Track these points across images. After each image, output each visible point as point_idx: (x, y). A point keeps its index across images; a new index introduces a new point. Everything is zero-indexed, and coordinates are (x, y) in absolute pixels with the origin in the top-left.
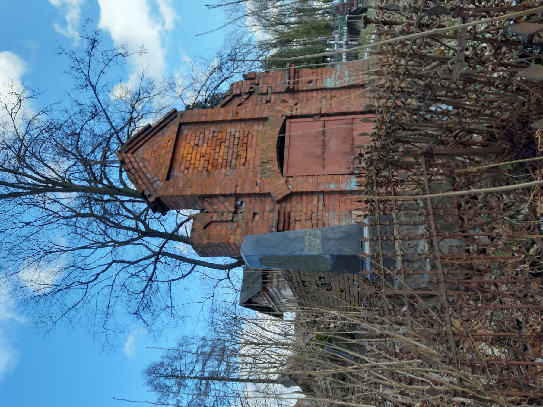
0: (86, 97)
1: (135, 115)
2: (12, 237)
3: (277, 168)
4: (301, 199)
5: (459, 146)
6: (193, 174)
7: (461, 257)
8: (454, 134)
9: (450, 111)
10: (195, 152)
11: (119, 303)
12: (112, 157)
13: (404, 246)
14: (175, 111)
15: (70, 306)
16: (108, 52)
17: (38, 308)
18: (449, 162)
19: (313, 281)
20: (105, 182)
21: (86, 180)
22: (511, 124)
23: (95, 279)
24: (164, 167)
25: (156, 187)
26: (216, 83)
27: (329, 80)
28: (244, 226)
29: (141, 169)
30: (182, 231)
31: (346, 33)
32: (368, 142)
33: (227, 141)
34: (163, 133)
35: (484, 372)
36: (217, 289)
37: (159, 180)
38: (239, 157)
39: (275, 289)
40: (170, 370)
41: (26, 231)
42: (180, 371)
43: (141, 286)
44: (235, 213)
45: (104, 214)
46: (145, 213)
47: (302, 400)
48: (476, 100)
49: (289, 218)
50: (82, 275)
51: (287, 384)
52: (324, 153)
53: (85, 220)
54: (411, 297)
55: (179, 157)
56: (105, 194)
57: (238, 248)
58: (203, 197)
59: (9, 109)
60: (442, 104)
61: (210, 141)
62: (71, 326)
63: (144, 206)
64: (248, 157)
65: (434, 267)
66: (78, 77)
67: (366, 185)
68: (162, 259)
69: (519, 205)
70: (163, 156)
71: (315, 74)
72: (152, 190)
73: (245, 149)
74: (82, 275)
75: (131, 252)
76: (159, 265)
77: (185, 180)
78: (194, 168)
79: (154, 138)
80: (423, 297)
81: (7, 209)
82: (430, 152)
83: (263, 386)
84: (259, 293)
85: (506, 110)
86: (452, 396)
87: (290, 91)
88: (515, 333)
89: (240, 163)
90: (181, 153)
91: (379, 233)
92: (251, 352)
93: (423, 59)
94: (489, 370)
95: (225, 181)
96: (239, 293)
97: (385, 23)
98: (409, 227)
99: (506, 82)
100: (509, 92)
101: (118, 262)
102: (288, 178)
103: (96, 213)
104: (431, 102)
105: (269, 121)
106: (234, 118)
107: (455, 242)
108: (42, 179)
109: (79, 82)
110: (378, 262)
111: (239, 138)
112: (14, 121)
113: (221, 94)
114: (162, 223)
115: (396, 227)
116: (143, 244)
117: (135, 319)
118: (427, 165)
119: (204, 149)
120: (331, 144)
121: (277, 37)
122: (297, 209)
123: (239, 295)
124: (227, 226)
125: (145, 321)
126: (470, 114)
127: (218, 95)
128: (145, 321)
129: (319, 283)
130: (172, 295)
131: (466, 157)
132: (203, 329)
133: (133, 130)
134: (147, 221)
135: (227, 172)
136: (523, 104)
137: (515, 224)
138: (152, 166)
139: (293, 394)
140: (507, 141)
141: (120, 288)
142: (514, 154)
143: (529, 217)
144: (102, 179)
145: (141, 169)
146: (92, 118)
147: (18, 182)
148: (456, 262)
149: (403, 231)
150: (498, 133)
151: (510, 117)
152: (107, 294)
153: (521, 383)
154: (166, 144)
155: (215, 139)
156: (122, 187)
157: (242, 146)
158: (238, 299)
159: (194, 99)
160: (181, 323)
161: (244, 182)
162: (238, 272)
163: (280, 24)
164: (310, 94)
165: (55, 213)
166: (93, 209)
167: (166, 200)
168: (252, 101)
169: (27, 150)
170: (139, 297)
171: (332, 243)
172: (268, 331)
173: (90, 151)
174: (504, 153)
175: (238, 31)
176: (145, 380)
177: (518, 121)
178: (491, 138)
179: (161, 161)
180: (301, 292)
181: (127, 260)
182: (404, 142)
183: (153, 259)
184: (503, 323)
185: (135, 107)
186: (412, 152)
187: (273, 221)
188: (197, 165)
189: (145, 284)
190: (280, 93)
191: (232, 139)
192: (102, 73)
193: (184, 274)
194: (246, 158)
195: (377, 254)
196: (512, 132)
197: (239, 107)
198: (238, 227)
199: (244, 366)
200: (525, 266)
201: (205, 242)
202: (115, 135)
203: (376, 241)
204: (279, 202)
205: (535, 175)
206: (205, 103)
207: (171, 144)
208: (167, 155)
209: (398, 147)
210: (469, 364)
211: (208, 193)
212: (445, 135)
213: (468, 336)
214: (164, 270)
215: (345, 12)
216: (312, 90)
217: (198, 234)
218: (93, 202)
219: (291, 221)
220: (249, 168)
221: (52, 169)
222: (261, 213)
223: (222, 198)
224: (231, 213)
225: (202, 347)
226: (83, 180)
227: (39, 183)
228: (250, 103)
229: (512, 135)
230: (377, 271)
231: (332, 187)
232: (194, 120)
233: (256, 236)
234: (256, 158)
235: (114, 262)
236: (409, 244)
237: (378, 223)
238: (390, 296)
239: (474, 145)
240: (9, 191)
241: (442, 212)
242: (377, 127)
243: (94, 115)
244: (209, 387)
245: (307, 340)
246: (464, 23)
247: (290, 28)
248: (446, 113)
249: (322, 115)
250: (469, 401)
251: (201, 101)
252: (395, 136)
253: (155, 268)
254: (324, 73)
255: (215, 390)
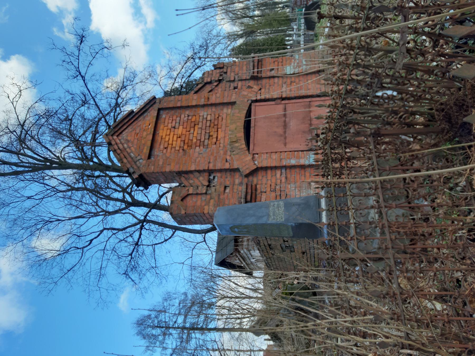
0: (77, 87)
1: (120, 100)
2: (16, 209)
3: (244, 146)
4: (266, 173)
5: (403, 126)
6: (171, 153)
7: (406, 225)
8: (399, 116)
9: (395, 96)
10: (172, 133)
11: (110, 264)
12: (100, 139)
13: (356, 214)
14: (154, 98)
15: (69, 268)
16: (95, 46)
17: (41, 270)
18: (394, 141)
19: (278, 244)
20: (95, 160)
21: (79, 159)
22: (448, 107)
23: (89, 244)
24: (146, 147)
25: (139, 165)
26: (190, 71)
27: (288, 68)
28: (216, 198)
29: (126, 149)
30: (163, 201)
31: (303, 25)
32: (322, 125)
33: (200, 124)
34: (144, 118)
35: (428, 326)
36: (195, 251)
37: (141, 159)
38: (211, 138)
39: (245, 250)
40: (156, 321)
41: (28, 203)
42: (165, 322)
43: (128, 250)
44: (208, 186)
45: (95, 187)
46: (131, 186)
47: (271, 345)
48: (417, 86)
49: (256, 190)
50: (78, 241)
51: (257, 333)
52: (285, 132)
53: (79, 194)
54: (363, 260)
55: (158, 138)
56: (95, 170)
57: (212, 217)
58: (180, 173)
59: (11, 98)
60: (387, 90)
61: (185, 124)
62: (70, 286)
63: (129, 180)
64: (219, 137)
65: (383, 233)
66: (69, 68)
67: (322, 161)
68: (147, 226)
69: (457, 179)
70: (145, 138)
71: (276, 63)
72: (135, 167)
73: (216, 130)
74: (78, 241)
75: (119, 221)
76: (143, 232)
77: (165, 158)
78: (172, 148)
79: (136, 122)
80: (374, 260)
81: (11, 185)
82: (377, 132)
83: (237, 334)
84: (232, 254)
85: (444, 94)
86: (399, 349)
87: (254, 78)
88: (455, 292)
89: (212, 142)
90: (160, 134)
91: (334, 204)
92: (227, 304)
93: (369, 51)
94: (432, 325)
95: (199, 159)
96: (214, 254)
97: (337, 17)
98: (361, 198)
99: (444, 70)
100: (446, 79)
101: (108, 229)
102: (255, 155)
103: (88, 187)
104: (378, 89)
105: (236, 105)
106: (206, 103)
107: (400, 212)
108: (39, 158)
109: (70, 73)
110: (334, 230)
111: (210, 121)
112: (15, 109)
113: (196, 80)
114: (146, 194)
115: (349, 198)
116: (130, 213)
117: (125, 278)
118: (376, 144)
119: (180, 131)
120: (291, 124)
121: (243, 28)
122: (263, 182)
123: (214, 256)
124: (201, 198)
125: (133, 281)
126: (413, 99)
127: (192, 82)
128: (133, 281)
129: (283, 246)
130: (156, 257)
131: (411, 136)
132: (184, 286)
133: (119, 114)
134: (133, 193)
135: (201, 151)
136: (460, 89)
137: (454, 196)
138: (135, 146)
139: (263, 342)
140: (446, 122)
141: (110, 252)
142: (452, 133)
143: (466, 189)
144: (92, 158)
145: (126, 149)
146: (82, 106)
147: (19, 161)
148: (402, 230)
149: (356, 201)
150: (439, 116)
151: (448, 100)
152: (100, 258)
153: (461, 336)
154: (147, 127)
155: (189, 122)
156: (110, 164)
157: (214, 127)
158: (214, 259)
159: (171, 85)
160: (164, 281)
161: (216, 160)
162: (213, 236)
163: (246, 17)
164: (272, 80)
165: (53, 187)
166: (86, 184)
167: (148, 176)
168: (221, 88)
169: (27, 133)
170: (127, 260)
171: (294, 209)
172: (240, 286)
173: (82, 133)
174: (443, 132)
175: (209, 25)
176: (135, 331)
177: (455, 104)
178: (431, 119)
179: (143, 142)
180: (268, 254)
181: (116, 227)
182: (354, 124)
183: (138, 226)
184: (445, 283)
185: (120, 94)
186: (362, 133)
187: (242, 193)
188: (174, 145)
189: (132, 248)
190: (246, 80)
191: (205, 121)
192: (90, 65)
193: (166, 238)
194: (217, 138)
195: (333, 222)
196: (450, 114)
197: (210, 93)
198: (211, 198)
199: (220, 317)
200: (464, 231)
201: (183, 212)
202: (103, 119)
203: (332, 211)
204: (247, 176)
205: (471, 152)
206: (181, 89)
207: (151, 127)
208: (148, 136)
209: (350, 128)
210: (414, 320)
211: (184, 169)
212: (391, 117)
213: (413, 295)
214: (148, 236)
215: (302, 6)
216: (274, 77)
217: (177, 205)
218: (85, 178)
219: (257, 193)
220: (220, 147)
221: (49, 150)
222: (231, 186)
223: (197, 173)
224: (205, 187)
225: (184, 301)
226: (76, 159)
227: (37, 162)
228: (220, 90)
229: (450, 116)
230: (333, 237)
231: (293, 162)
232: (171, 105)
233: (228, 208)
234: (226, 139)
235: (105, 229)
236: (361, 214)
237: (334, 196)
238: (345, 260)
239: (417, 125)
240: (13, 169)
241: (389, 186)
242: (331, 111)
243: (84, 103)
244: (191, 336)
245: (274, 294)
246: (405, 22)
247: (254, 20)
248: (391, 98)
249: (283, 99)
250: (415, 353)
251: (178, 87)
252: (346, 119)
253: (141, 234)
254: (284, 62)
255: (196, 338)
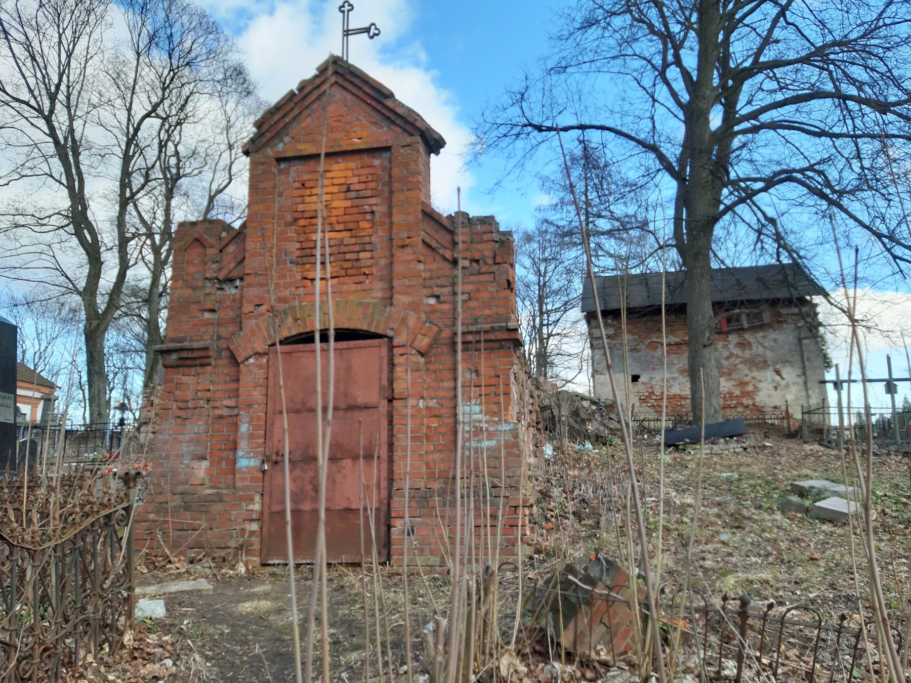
3: (285, 333)
27: (477, 409)
33: (353, 241)
49: (202, 365)
61: (355, 210)
79: (368, 109)
111: (358, 260)
124: (198, 272)
188: (308, 199)
191: (357, 248)
219: (198, 368)
